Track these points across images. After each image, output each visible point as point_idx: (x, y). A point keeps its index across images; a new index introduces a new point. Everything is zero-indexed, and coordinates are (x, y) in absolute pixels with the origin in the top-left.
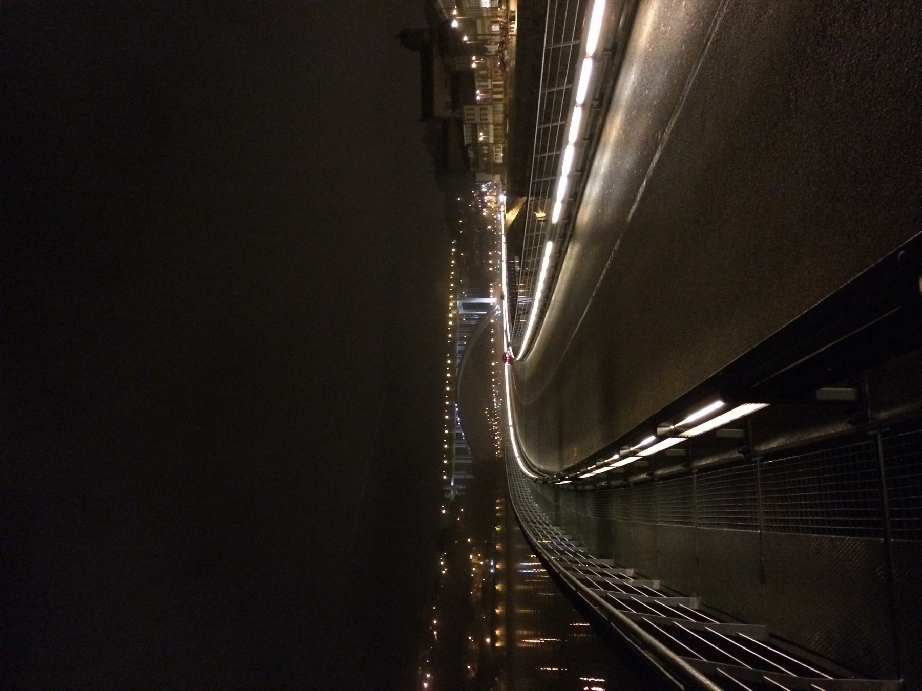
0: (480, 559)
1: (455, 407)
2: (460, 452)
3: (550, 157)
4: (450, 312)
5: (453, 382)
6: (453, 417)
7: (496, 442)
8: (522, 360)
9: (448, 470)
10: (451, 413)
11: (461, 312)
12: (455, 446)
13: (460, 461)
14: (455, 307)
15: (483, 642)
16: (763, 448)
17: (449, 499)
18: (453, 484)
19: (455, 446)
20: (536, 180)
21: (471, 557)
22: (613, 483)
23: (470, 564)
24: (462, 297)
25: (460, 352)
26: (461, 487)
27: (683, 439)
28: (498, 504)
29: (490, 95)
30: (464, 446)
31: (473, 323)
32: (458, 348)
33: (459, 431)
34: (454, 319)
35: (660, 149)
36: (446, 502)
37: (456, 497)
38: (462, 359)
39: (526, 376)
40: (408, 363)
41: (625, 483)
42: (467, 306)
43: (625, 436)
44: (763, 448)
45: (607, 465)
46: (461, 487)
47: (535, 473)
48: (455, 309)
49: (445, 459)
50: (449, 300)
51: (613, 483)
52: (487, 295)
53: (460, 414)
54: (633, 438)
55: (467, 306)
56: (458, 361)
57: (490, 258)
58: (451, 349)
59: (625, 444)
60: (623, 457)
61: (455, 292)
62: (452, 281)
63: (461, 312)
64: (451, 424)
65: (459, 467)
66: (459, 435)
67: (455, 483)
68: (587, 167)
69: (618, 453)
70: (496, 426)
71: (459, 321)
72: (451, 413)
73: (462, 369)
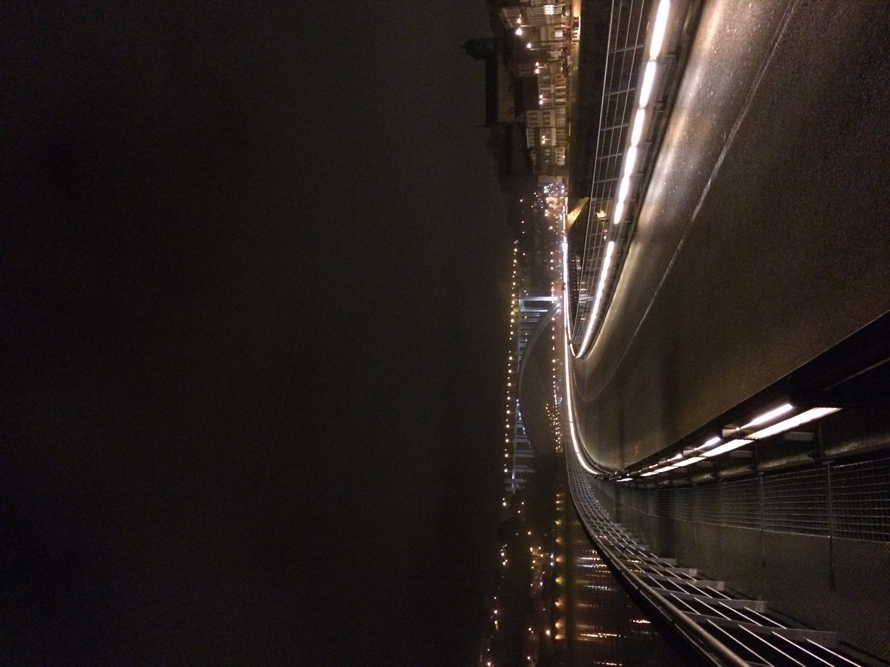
0: (540, 552)
1: (516, 403)
2: (520, 446)
3: (612, 159)
4: (512, 310)
6: (514, 412)
10: (513, 408)
11: (523, 310)
12: (516, 455)
14: (517, 306)
15: (543, 634)
17: (510, 492)
18: (514, 477)
20: (599, 182)
21: (531, 549)
23: (530, 557)
24: (524, 296)
26: (522, 481)
27: (749, 442)
29: (553, 100)
30: (525, 441)
31: (535, 321)
32: (520, 345)
33: (520, 426)
34: (515, 317)
35: (725, 150)
36: (506, 494)
37: (517, 491)
38: (523, 356)
39: (587, 374)
40: (471, 359)
45: (670, 464)
46: (522, 481)
47: (595, 469)
49: (508, 409)
50: (512, 298)
52: (549, 294)
53: (521, 410)
54: (697, 438)
56: (520, 358)
58: (513, 346)
59: (688, 445)
60: (686, 457)
61: (516, 291)
62: (512, 329)
63: (523, 310)
64: (513, 419)
65: (520, 461)
67: (516, 476)
68: (650, 168)
72: (513, 408)
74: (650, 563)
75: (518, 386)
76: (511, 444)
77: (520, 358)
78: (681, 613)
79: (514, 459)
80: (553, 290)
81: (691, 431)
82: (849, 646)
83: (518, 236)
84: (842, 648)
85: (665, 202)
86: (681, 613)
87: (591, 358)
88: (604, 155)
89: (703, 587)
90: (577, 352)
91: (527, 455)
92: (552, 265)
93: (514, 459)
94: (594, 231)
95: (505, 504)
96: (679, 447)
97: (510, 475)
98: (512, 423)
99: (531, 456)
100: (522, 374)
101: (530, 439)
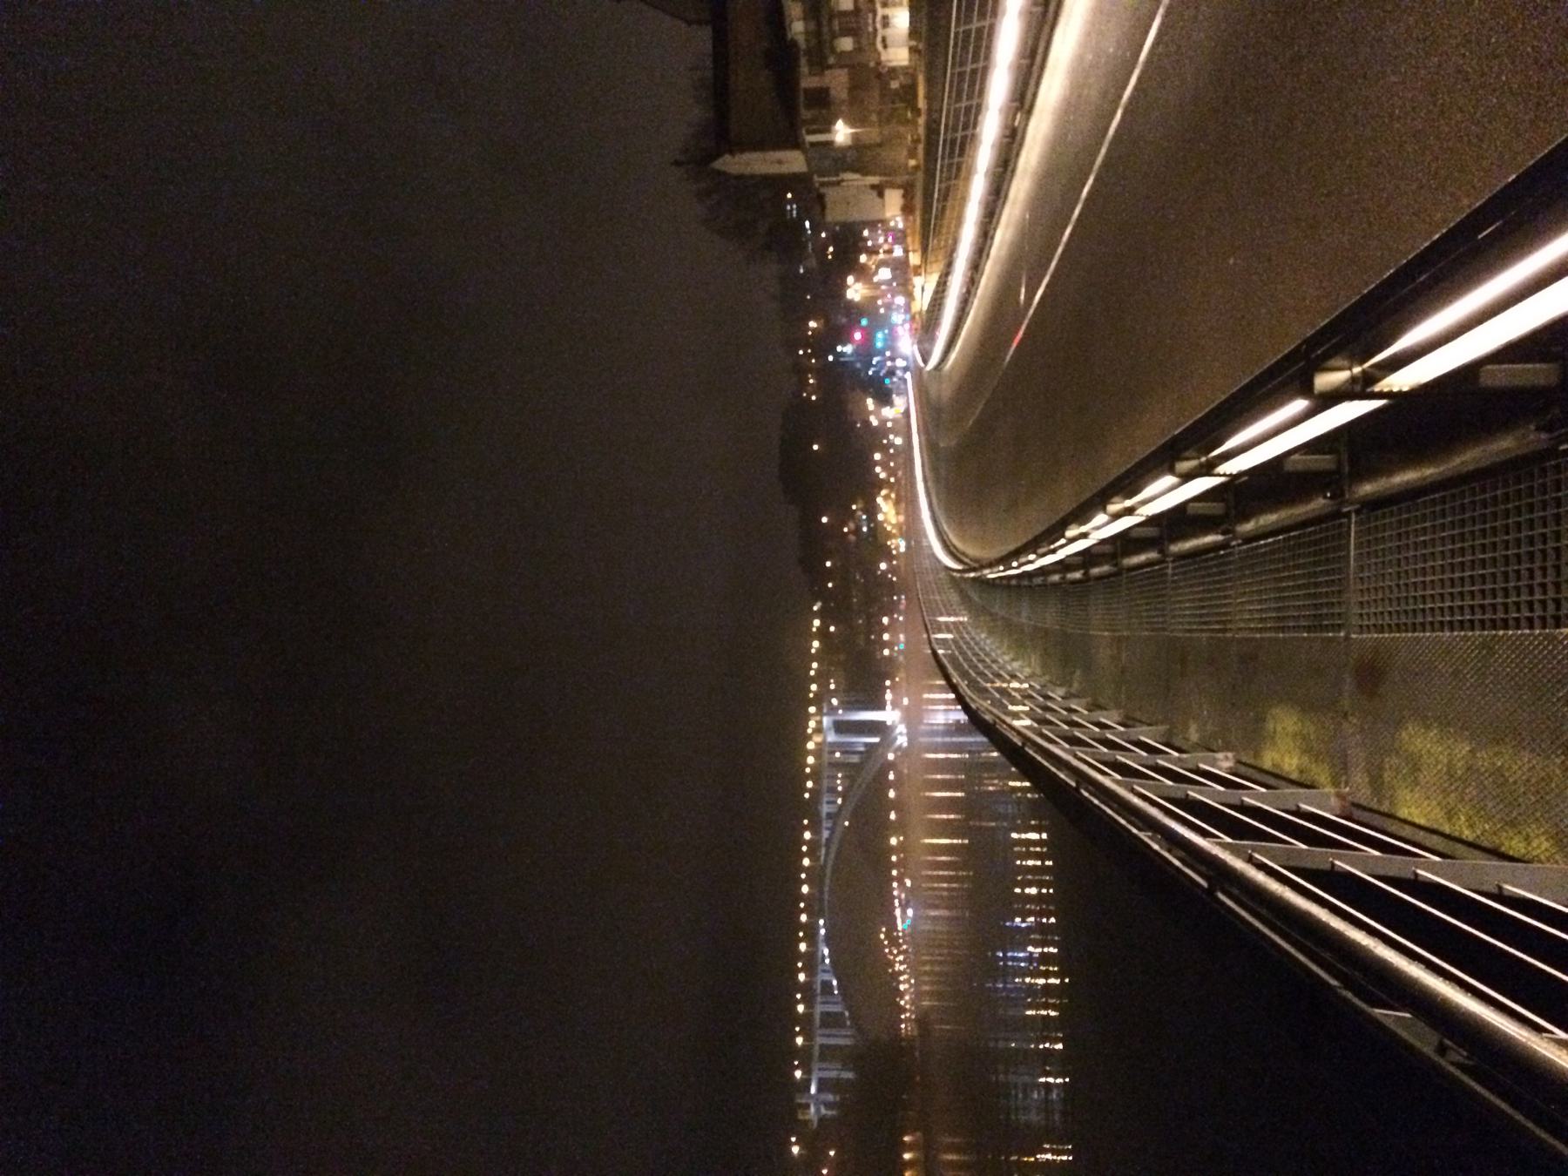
1: (817, 928)
2: (831, 1021)
3: (980, 31)
4: (809, 738)
5: (815, 877)
6: (817, 947)
7: (901, 995)
8: (938, 368)
9: (805, 1057)
10: (811, 937)
11: (832, 737)
12: (819, 1009)
13: (832, 1041)
14: (818, 730)
16: (1367, 489)
17: (806, 1123)
18: (816, 1106)
19: (819, 1009)
20: (958, 70)
22: (1095, 571)
24: (833, 710)
25: (829, 815)
26: (830, 1097)
27: (1222, 479)
28: (910, 1148)
31: (855, 759)
32: (825, 809)
33: (826, 977)
34: (817, 753)
35: (1161, 11)
36: (800, 1128)
37: (822, 1120)
38: (832, 830)
39: (945, 391)
41: (1114, 569)
42: (841, 727)
43: (1120, 479)
44: (1367, 489)
46: (830, 1097)
47: (960, 561)
48: (820, 730)
51: (1095, 571)
52: (880, 706)
54: (1129, 483)
55: (841, 727)
56: (826, 834)
57: (885, 629)
58: (811, 809)
59: (1116, 494)
62: (813, 680)
63: (832, 737)
64: (811, 961)
65: (828, 1053)
66: (827, 986)
67: (819, 1090)
68: (1041, 50)
69: (1104, 510)
70: (901, 963)
71: (826, 757)
73: (834, 848)
74: (1047, 709)
75: (821, 892)
76: (807, 1050)
77: (826, 834)
78: (1099, 777)
79: (817, 1017)
80: (889, 696)
81: (1116, 472)
82: (1364, 809)
83: (822, 594)
84: (1357, 813)
85: (1070, 108)
86: (1099, 777)
87: (953, 368)
88: (966, 23)
89: (1134, 738)
90: (925, 361)
91: (842, 1039)
92: (885, 645)
93: (817, 1017)
94: (955, 130)
95: (795, 1150)
96: (1098, 502)
97: (805, 1084)
98: (810, 969)
99: (848, 1042)
100: (828, 871)
101: (849, 1008)
